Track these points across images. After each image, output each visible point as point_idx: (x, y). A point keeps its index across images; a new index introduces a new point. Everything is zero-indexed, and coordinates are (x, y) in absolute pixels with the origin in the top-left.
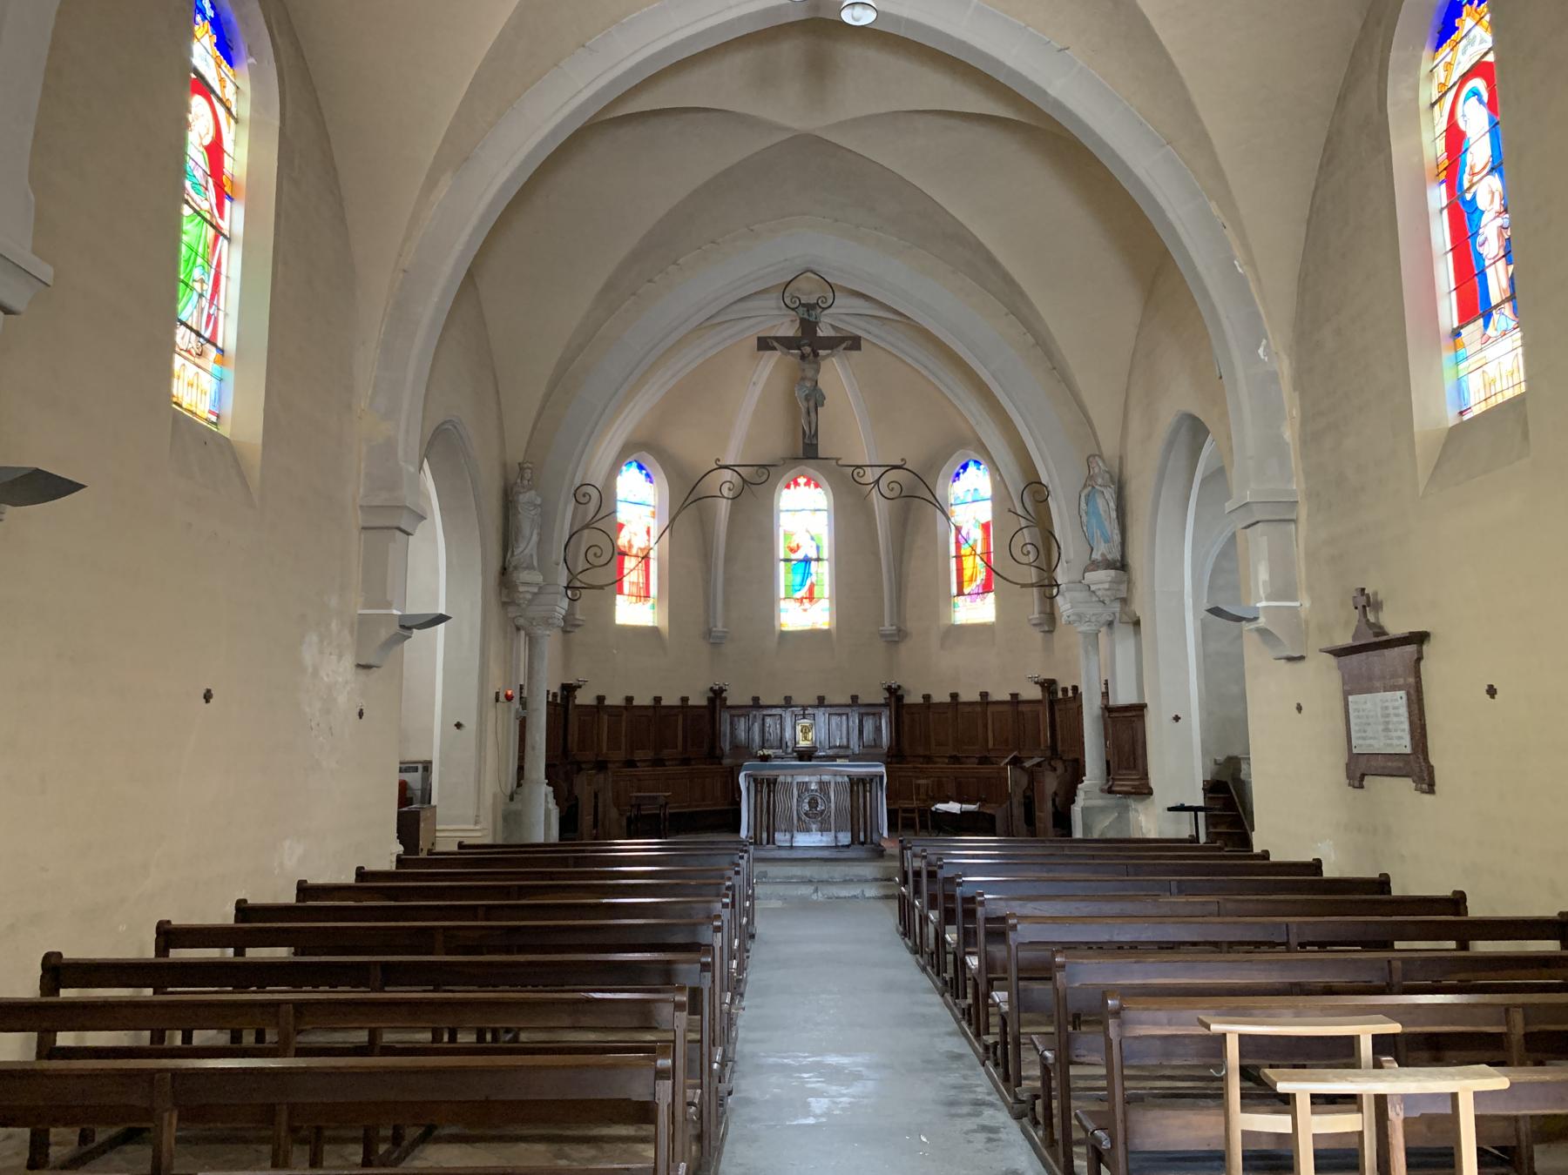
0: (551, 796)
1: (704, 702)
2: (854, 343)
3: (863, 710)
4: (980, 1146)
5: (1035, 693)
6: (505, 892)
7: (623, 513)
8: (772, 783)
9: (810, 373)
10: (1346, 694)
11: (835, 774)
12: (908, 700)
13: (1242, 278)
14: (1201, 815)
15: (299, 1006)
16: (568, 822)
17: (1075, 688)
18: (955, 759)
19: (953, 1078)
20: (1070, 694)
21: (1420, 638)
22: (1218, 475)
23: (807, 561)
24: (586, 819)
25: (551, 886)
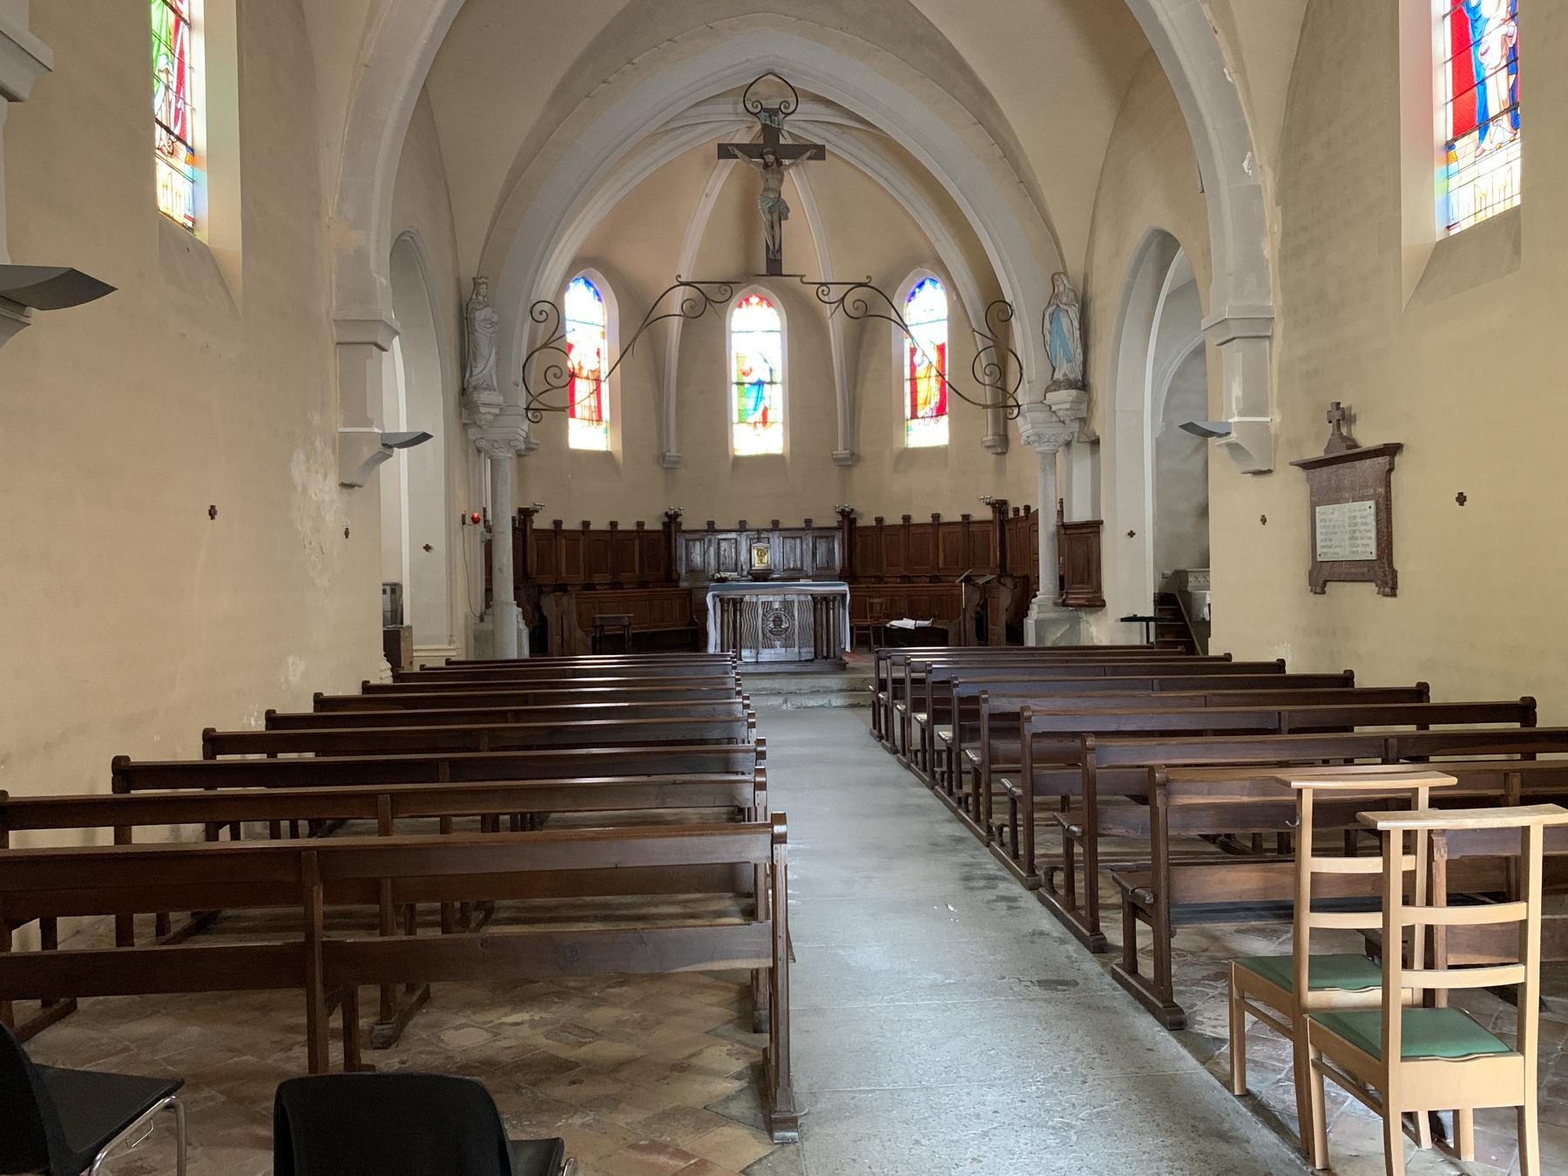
1: (659, 527)
2: (819, 153)
3: (817, 533)
4: (1003, 913)
5: (986, 514)
12: (860, 523)
13: (1231, 86)
14: (1152, 624)
15: (394, 795)
16: (538, 640)
17: (1027, 508)
18: (906, 579)
19: (964, 858)
20: (1022, 513)
21: (1392, 450)
22: (1188, 290)
23: (760, 384)
24: (554, 639)
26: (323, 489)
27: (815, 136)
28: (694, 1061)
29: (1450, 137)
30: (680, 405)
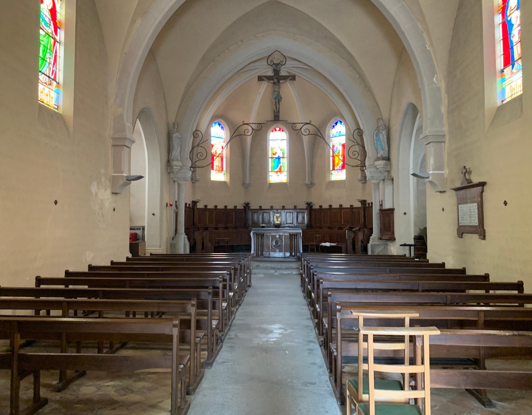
0: (186, 239)
1: (242, 208)
3: (298, 211)
5: (359, 205)
6: (157, 269)
7: (213, 141)
8: (262, 235)
9: (276, 89)
10: (458, 204)
11: (284, 232)
12: (314, 207)
13: (429, 51)
14: (412, 248)
16: (193, 248)
17: (372, 203)
18: (330, 228)
21: (483, 184)
23: (279, 158)
24: (199, 246)
25: (174, 268)
26: (105, 195)
27: (294, 72)
28: (160, 404)
29: (502, 68)
30: (251, 165)
